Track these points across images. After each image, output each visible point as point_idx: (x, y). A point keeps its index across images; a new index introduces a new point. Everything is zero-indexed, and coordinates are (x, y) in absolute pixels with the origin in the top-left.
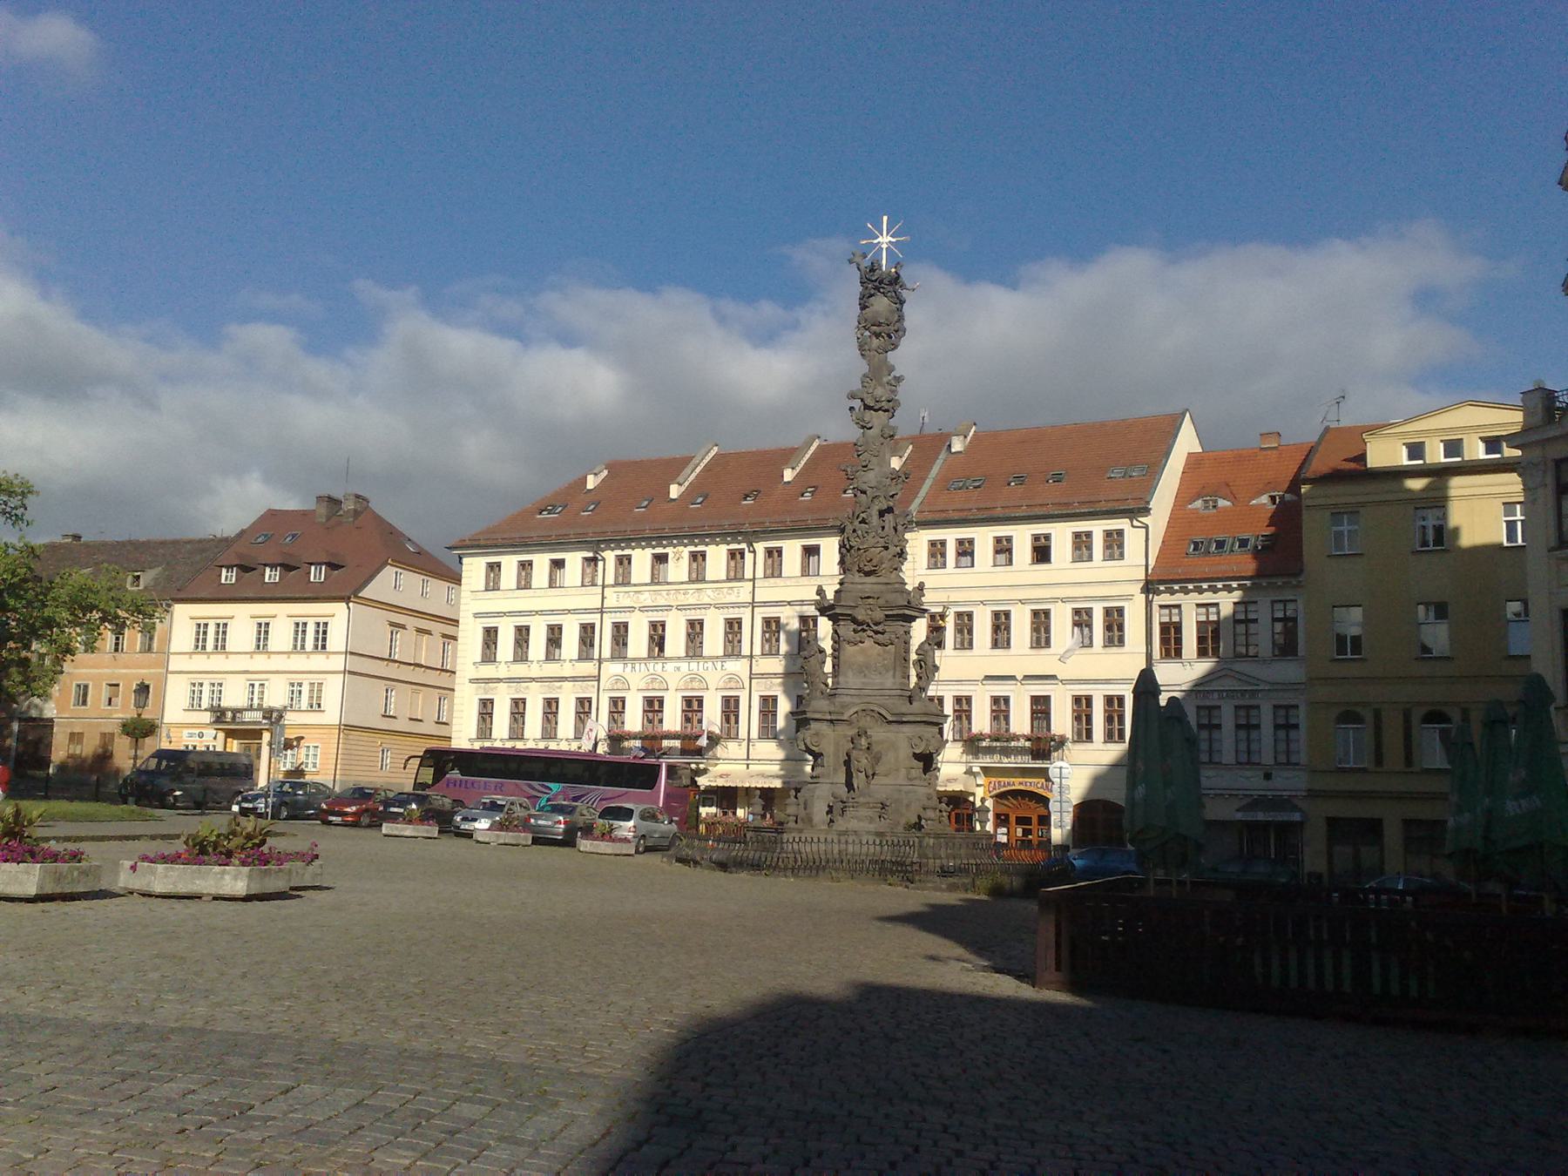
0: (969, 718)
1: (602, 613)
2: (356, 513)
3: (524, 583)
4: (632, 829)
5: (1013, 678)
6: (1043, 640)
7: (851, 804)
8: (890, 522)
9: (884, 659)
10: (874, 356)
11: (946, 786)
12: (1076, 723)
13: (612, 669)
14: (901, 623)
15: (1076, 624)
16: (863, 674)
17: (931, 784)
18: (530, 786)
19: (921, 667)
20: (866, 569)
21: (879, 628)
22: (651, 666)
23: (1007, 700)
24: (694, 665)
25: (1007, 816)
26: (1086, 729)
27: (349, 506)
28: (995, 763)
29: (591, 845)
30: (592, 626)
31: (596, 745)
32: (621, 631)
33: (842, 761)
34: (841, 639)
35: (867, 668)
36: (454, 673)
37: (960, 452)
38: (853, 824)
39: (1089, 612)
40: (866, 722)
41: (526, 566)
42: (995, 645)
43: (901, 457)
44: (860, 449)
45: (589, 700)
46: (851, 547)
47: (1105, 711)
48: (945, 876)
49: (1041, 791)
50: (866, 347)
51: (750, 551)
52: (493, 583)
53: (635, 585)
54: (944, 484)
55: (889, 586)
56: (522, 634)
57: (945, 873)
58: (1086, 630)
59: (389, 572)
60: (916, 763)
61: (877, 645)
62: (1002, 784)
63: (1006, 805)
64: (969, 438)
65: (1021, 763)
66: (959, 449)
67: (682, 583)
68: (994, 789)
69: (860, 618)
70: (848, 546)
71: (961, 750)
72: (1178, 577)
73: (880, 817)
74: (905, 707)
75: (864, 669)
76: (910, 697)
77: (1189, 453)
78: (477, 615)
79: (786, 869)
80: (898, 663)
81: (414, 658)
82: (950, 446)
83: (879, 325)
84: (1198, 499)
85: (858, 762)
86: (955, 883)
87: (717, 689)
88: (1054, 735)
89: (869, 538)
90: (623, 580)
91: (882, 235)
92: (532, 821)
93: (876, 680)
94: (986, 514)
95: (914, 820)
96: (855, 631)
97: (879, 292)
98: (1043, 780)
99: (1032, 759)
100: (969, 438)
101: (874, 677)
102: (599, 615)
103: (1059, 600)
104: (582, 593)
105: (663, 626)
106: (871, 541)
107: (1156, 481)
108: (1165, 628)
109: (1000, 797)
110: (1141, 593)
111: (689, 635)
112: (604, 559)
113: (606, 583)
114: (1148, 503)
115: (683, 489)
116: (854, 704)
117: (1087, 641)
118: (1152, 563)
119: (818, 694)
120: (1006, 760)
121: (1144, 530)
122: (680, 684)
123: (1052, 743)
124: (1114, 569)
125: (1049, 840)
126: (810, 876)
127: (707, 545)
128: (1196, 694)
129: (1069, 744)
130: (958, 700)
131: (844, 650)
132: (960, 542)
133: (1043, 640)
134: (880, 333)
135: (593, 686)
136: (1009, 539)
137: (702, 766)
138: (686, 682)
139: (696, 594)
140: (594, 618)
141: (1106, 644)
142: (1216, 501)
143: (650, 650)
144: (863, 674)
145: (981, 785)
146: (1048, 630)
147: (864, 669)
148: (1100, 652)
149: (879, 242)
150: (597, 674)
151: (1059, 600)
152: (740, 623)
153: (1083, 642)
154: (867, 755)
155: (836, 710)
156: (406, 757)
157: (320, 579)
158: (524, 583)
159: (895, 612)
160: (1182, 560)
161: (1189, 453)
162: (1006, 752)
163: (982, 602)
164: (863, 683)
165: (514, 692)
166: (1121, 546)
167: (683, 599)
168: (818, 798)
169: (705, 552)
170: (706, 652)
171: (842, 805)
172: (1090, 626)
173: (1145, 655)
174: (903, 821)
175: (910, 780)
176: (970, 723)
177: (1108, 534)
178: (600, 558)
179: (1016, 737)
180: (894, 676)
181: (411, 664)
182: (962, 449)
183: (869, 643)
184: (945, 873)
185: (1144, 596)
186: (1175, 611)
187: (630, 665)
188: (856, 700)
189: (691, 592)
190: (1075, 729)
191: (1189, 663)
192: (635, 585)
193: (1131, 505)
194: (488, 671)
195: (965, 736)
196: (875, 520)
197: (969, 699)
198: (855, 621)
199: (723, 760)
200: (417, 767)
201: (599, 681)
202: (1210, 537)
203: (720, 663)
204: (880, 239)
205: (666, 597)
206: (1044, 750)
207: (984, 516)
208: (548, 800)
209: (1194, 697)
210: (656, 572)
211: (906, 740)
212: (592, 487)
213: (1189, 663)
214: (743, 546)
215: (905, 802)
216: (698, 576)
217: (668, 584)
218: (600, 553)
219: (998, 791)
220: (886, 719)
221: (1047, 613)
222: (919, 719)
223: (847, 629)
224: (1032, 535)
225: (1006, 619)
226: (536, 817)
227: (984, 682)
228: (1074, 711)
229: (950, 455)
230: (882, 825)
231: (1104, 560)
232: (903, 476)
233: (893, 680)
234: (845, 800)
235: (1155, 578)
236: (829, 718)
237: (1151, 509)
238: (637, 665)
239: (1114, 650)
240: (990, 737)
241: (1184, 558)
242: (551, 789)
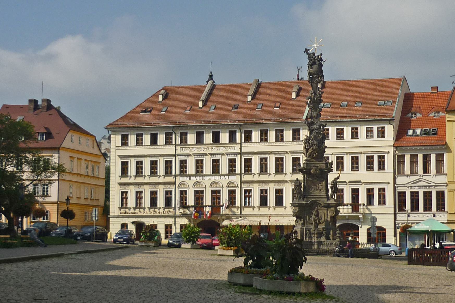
5: (345, 182)
13: (180, 180)
24: (216, 177)
32: (183, 164)
39: (372, 157)
78: (180, 152)
124: (381, 142)
148: (377, 172)
152: (235, 161)
157: (43, 139)
239: (382, 171)
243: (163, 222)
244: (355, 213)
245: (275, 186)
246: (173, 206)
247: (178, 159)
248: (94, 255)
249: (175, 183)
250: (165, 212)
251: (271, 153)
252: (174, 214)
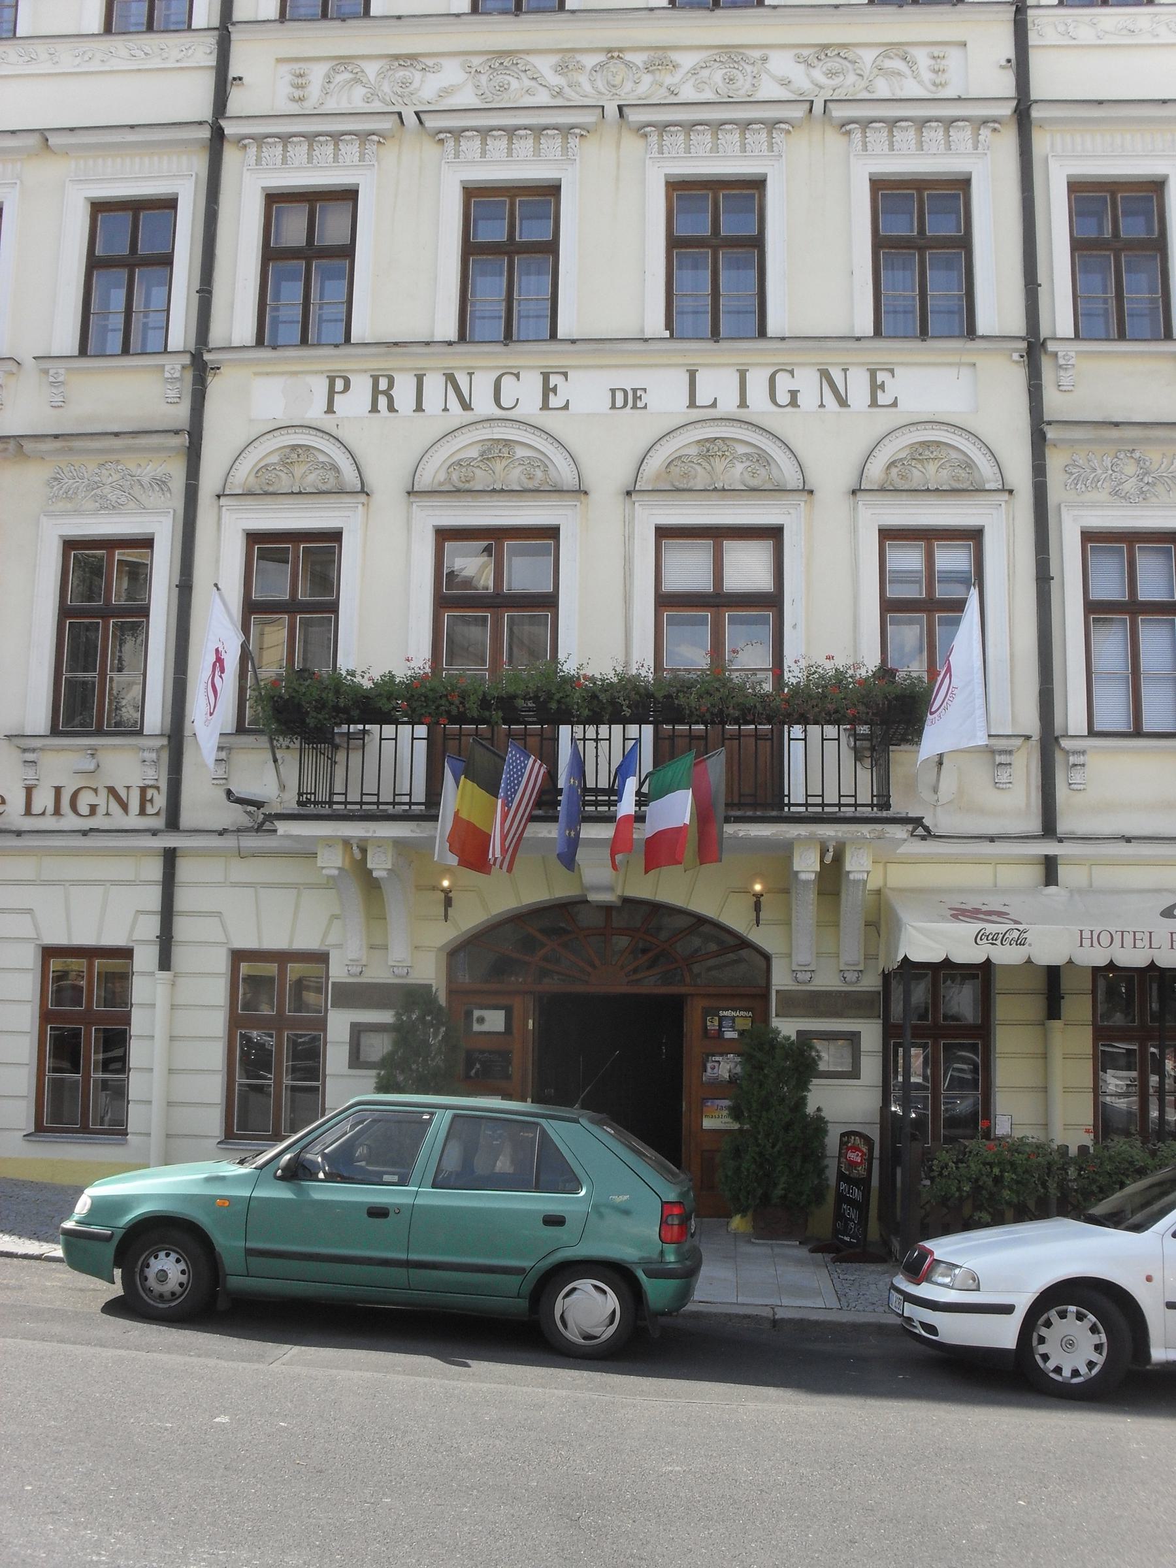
205: (555, 80)
243: (21, 926)
245: (110, 1055)
246: (155, 717)
248: (976, 832)
250: (43, 800)
252: (159, 823)
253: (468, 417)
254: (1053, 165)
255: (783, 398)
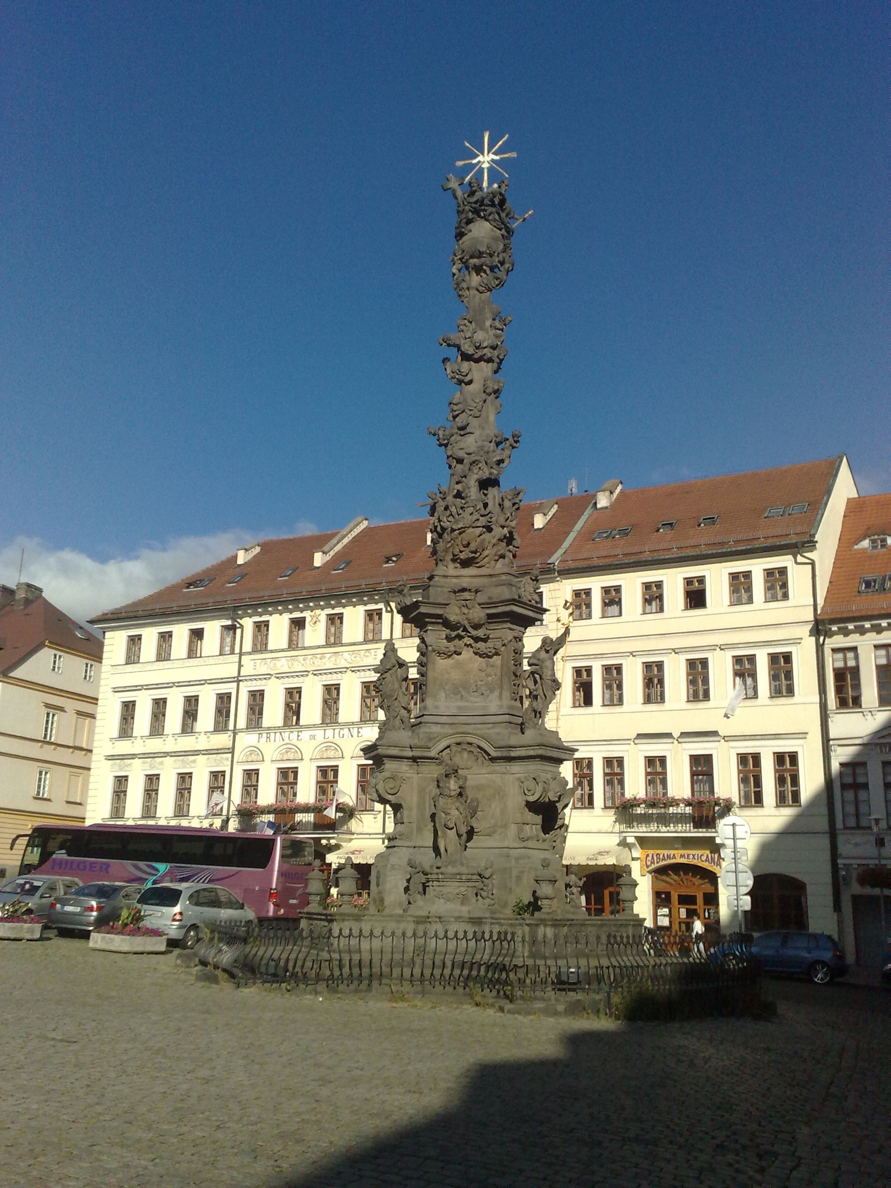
0: (621, 782)
1: (238, 681)
2: (27, 602)
3: (163, 655)
4: (178, 917)
5: (668, 735)
6: (701, 693)
7: (435, 876)
8: (494, 497)
9: (488, 675)
10: (474, 296)
11: (596, 860)
12: (742, 786)
13: (246, 740)
14: (509, 625)
15: (738, 674)
16: (459, 696)
17: (558, 848)
18: (137, 868)
19: (536, 682)
20: (462, 556)
21: (480, 633)
22: (286, 735)
23: (663, 760)
24: (329, 732)
25: (668, 894)
26: (755, 792)
27: (21, 595)
28: (651, 832)
29: (103, 938)
30: (229, 696)
31: (226, 822)
32: (257, 699)
33: (428, 815)
34: (430, 648)
35: (465, 688)
36: (91, 751)
37: (606, 508)
38: (440, 907)
39: (752, 659)
40: (461, 759)
41: (166, 638)
42: (648, 700)
43: (545, 515)
44: (455, 408)
45: (223, 773)
46: (444, 529)
47: (776, 771)
48: (564, 990)
49: (706, 865)
50: (464, 285)
51: (387, 611)
52: (132, 656)
53: (272, 651)
54: (588, 536)
55: (494, 579)
56: (160, 706)
57: (562, 984)
58: (749, 681)
59: (46, 655)
60: (530, 816)
61: (477, 657)
62: (661, 857)
63: (667, 882)
64: (615, 495)
65: (681, 832)
66: (605, 505)
67: (319, 647)
68: (652, 862)
69: (453, 618)
70: (439, 529)
71: (613, 819)
72: (851, 615)
73: (476, 894)
74: (516, 739)
75: (461, 689)
76: (522, 724)
77: (848, 499)
78: (116, 690)
79: (318, 978)
80: (505, 680)
81: (74, 741)
82: (595, 504)
83: (480, 255)
84: (865, 539)
85: (447, 814)
86: (579, 1001)
87: (352, 757)
88: (719, 799)
89: (466, 514)
90: (261, 645)
91: (483, 155)
92: (58, 906)
93: (476, 703)
94: (632, 559)
95: (527, 898)
96: (449, 639)
97: (479, 216)
98: (708, 852)
99: (694, 828)
100: (615, 495)
101: (476, 700)
102: (236, 683)
103: (717, 648)
104: (220, 662)
105: (300, 693)
106: (467, 518)
107: (819, 516)
108: (840, 675)
109: (660, 872)
110: (810, 636)
111: (325, 701)
112: (242, 627)
113: (243, 651)
114: (814, 536)
115: (328, 557)
116: (446, 736)
117: (751, 692)
118: (821, 602)
119: (398, 722)
120: (664, 829)
121: (810, 566)
122: (315, 754)
123: (717, 808)
124: (778, 611)
125: (718, 921)
126: (357, 991)
127: (344, 607)
128: (881, 748)
129: (735, 809)
130: (608, 762)
131: (434, 663)
132: (606, 590)
133: (701, 693)
134: (482, 266)
135: (227, 759)
136: (659, 585)
137: (333, 842)
138: (321, 751)
139: (333, 659)
140: (231, 688)
141: (773, 695)
142: (884, 540)
143: (286, 718)
144: (459, 696)
145: (637, 859)
146: (706, 681)
147: (461, 689)
149: (479, 162)
150: (231, 746)
151: (717, 648)
153: (746, 694)
154: (458, 804)
155: (419, 744)
156: (14, 836)
158: (163, 655)
159: (500, 610)
160: (854, 599)
161: (848, 499)
162: (665, 820)
163: (631, 653)
164: (459, 708)
165: (148, 768)
166: (784, 586)
167: (320, 664)
168: (393, 867)
169: (342, 614)
170: (342, 718)
171: (423, 879)
172: (754, 676)
173: (818, 705)
174: (512, 900)
175: (523, 840)
176: (623, 788)
177: (769, 573)
178: (238, 625)
179: (675, 802)
180: (500, 697)
181: (69, 747)
182: (608, 505)
183: (467, 654)
184: (562, 984)
185: (813, 639)
186: (850, 655)
187: (265, 735)
188: (448, 730)
189: (328, 656)
190: (742, 793)
191: (870, 711)
192: (272, 651)
193: (793, 540)
194: (124, 747)
195: (618, 802)
196: (473, 492)
197: (620, 761)
198: (447, 624)
199: (357, 834)
200: (24, 847)
201: (233, 753)
202: (883, 574)
203: (356, 730)
204: (480, 158)
205: (303, 662)
206: (707, 817)
207: (632, 561)
208: (154, 882)
209: (879, 751)
210: (295, 638)
211: (517, 783)
212: (242, 562)
213: (870, 711)
214: (381, 606)
215: (515, 873)
216: (334, 639)
217: (304, 648)
218: (239, 620)
219: (656, 865)
220: (489, 755)
221: (704, 663)
222: (532, 753)
223: (437, 636)
224: (685, 579)
225: (658, 671)
226: (65, 903)
227: (636, 741)
228: (739, 772)
229: (596, 512)
230: (478, 908)
231: (766, 602)
232: (511, 439)
233: (499, 703)
234: (428, 869)
235: (826, 617)
236: (410, 754)
237: (816, 542)
238: (272, 735)
239: (783, 700)
240: (645, 801)
241: (855, 596)
242: (157, 870)
244: (701, 830)
247: (245, 688)
249: (232, 751)
251: (206, 682)
253: (284, 743)
254: (795, 648)
255: (341, 736)
